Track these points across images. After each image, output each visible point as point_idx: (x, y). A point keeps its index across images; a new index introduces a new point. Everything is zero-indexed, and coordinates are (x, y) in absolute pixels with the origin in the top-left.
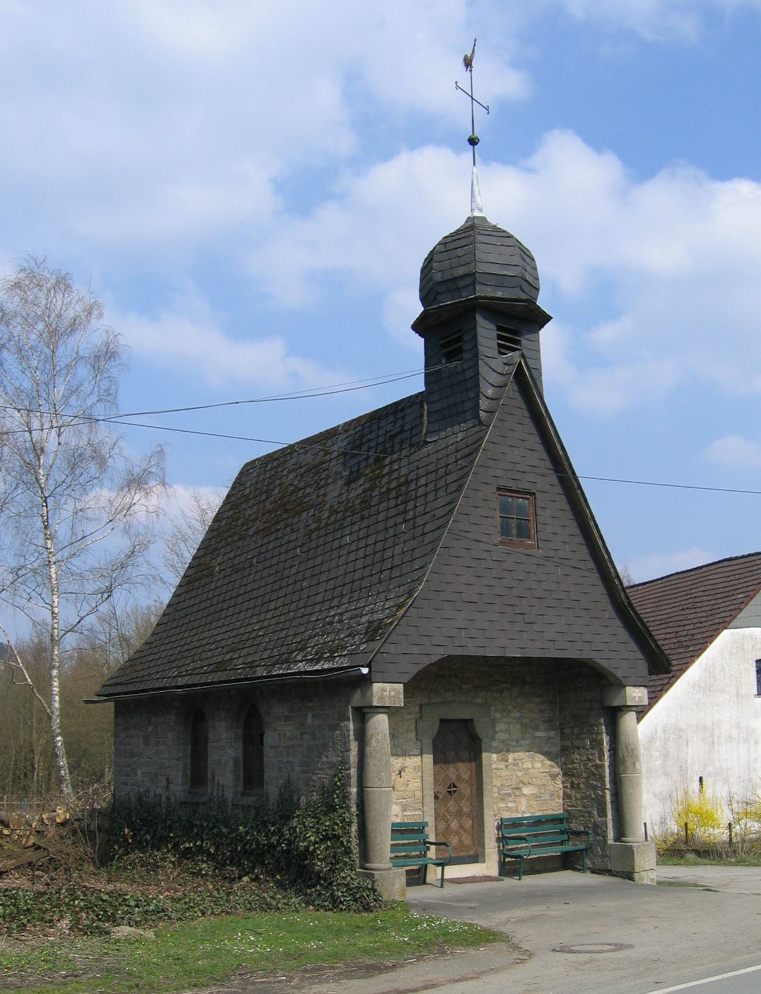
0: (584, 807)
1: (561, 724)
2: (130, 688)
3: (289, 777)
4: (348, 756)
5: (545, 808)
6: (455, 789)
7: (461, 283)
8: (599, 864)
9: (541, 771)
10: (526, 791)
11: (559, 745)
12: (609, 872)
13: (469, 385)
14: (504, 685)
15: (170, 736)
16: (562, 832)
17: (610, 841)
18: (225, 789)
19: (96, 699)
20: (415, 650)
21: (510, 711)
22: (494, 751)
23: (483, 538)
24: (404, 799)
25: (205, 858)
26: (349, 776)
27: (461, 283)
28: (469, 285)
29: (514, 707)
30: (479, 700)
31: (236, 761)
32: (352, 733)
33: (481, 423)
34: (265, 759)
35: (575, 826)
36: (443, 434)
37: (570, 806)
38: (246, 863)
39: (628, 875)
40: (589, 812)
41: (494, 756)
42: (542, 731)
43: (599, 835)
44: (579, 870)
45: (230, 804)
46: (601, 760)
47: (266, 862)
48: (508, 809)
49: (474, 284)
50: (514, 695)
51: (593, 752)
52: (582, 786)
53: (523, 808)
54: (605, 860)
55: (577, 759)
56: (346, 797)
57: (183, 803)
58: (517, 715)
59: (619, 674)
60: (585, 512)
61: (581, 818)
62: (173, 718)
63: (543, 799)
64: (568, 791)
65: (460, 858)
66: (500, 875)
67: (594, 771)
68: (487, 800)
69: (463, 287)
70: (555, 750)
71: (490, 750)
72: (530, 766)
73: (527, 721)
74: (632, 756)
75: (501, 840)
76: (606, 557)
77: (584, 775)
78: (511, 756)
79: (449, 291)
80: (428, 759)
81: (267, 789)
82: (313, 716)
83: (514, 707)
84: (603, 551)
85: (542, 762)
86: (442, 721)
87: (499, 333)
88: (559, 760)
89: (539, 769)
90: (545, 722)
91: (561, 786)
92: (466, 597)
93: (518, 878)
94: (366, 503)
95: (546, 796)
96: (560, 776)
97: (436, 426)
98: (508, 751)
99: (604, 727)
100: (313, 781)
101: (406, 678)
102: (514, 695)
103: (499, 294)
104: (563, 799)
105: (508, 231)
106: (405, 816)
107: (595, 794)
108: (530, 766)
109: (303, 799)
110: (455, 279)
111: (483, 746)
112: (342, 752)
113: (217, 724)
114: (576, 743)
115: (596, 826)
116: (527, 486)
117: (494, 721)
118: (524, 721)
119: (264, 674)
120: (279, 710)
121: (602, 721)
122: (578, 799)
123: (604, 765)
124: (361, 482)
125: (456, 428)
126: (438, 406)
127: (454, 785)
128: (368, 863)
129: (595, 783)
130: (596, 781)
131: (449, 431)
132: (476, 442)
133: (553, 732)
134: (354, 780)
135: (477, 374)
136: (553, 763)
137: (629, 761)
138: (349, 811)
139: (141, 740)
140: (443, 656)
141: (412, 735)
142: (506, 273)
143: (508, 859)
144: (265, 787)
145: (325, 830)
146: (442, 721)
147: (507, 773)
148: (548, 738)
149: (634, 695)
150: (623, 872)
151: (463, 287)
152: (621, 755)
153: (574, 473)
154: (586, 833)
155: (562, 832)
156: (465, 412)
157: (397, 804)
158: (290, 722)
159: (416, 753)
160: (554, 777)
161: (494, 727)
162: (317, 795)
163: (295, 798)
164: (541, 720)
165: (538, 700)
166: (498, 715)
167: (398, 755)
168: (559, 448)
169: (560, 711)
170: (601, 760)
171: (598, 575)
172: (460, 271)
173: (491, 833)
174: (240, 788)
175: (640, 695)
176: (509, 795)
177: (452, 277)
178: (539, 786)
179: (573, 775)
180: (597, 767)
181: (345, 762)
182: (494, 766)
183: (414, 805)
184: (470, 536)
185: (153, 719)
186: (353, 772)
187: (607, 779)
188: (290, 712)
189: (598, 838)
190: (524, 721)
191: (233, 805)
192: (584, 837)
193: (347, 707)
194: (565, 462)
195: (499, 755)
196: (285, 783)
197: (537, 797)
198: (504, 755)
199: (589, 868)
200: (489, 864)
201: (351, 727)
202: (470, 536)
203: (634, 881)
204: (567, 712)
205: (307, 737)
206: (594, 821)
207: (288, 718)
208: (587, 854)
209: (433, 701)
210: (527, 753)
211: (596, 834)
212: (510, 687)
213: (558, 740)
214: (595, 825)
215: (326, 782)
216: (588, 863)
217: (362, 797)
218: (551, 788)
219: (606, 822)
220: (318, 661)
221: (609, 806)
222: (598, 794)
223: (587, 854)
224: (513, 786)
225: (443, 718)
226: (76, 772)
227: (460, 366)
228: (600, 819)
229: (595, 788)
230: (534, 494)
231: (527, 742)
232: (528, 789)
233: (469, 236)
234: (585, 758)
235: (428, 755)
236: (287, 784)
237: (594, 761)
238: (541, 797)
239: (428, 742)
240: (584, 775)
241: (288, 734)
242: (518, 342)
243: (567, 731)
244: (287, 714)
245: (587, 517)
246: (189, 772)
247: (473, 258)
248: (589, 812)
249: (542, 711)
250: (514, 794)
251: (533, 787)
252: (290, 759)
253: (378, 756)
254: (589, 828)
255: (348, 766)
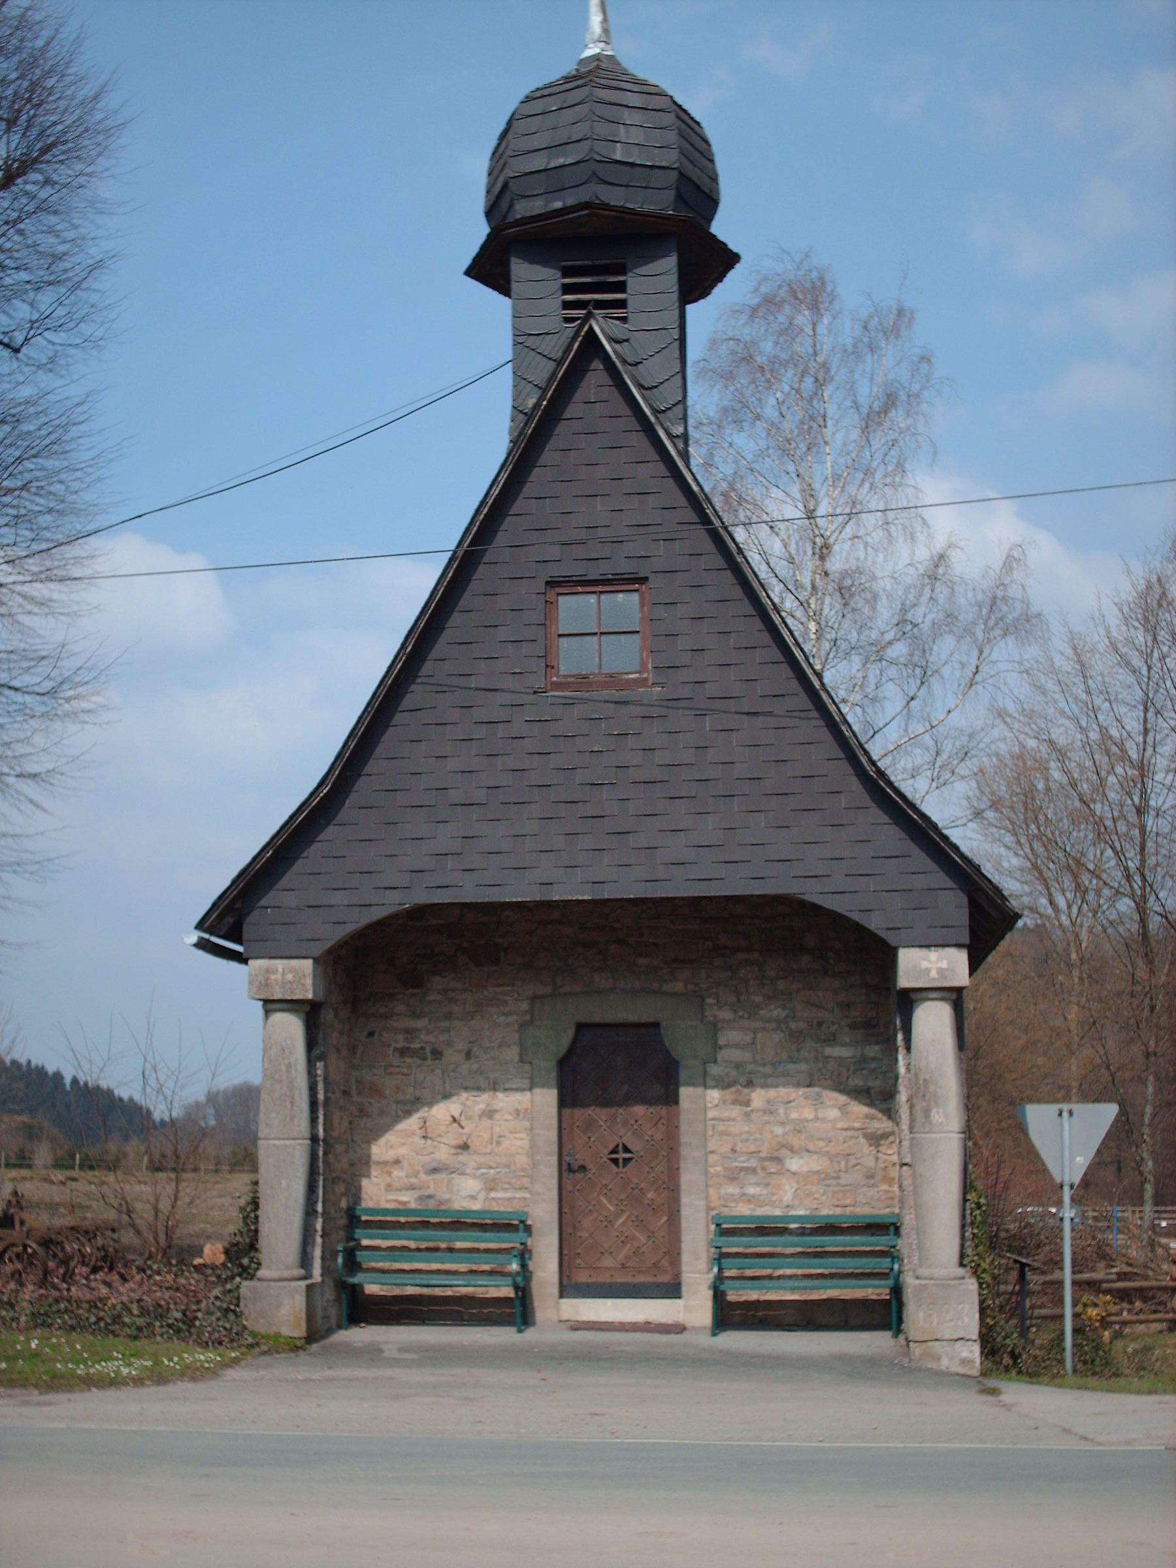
5: (848, 1202)
6: (627, 1155)
9: (839, 1125)
14: (741, 956)
20: (338, 898)
21: (758, 1006)
22: (713, 1083)
23: (508, 683)
24: (491, 1168)
29: (770, 998)
30: (678, 987)
41: (714, 1095)
42: (844, 1045)
48: (750, 1199)
53: (788, 1198)
58: (777, 1012)
63: (842, 1182)
65: (634, 1286)
71: (704, 1081)
73: (802, 1025)
74: (924, 1096)
78: (759, 1097)
80: (547, 1098)
85: (842, 1108)
86: (581, 1027)
87: (567, 280)
89: (834, 1121)
90: (853, 1026)
92: (455, 796)
98: (750, 1084)
101: (319, 949)
102: (772, 974)
106: (494, 1199)
108: (811, 1116)
111: (683, 1076)
116: (626, 567)
117: (715, 1028)
118: (793, 1025)
127: (613, 1152)
133: (877, 1048)
136: (873, 1111)
140: (401, 908)
141: (513, 1053)
142: (561, 161)
146: (581, 1027)
147: (746, 1128)
149: (925, 964)
157: (475, 1177)
159: (524, 1086)
164: (843, 1023)
165: (837, 984)
166: (725, 1014)
167: (478, 1089)
175: (944, 965)
176: (753, 1170)
178: (831, 1157)
182: (710, 1114)
183: (514, 1181)
184: (473, 682)
190: (793, 1025)
195: (727, 1091)
197: (822, 1177)
198: (739, 1092)
200: (692, 1303)
202: (473, 682)
209: (562, 990)
210: (801, 1091)
212: (761, 960)
218: (869, 1162)
224: (762, 1155)
225: (583, 1020)
226: (775, 1198)
231: (803, 1067)
232: (801, 1161)
235: (545, 1091)
238: (838, 1178)
239: (547, 1065)
242: (621, 287)
249: (846, 1006)
250: (764, 1169)
251: (815, 1157)
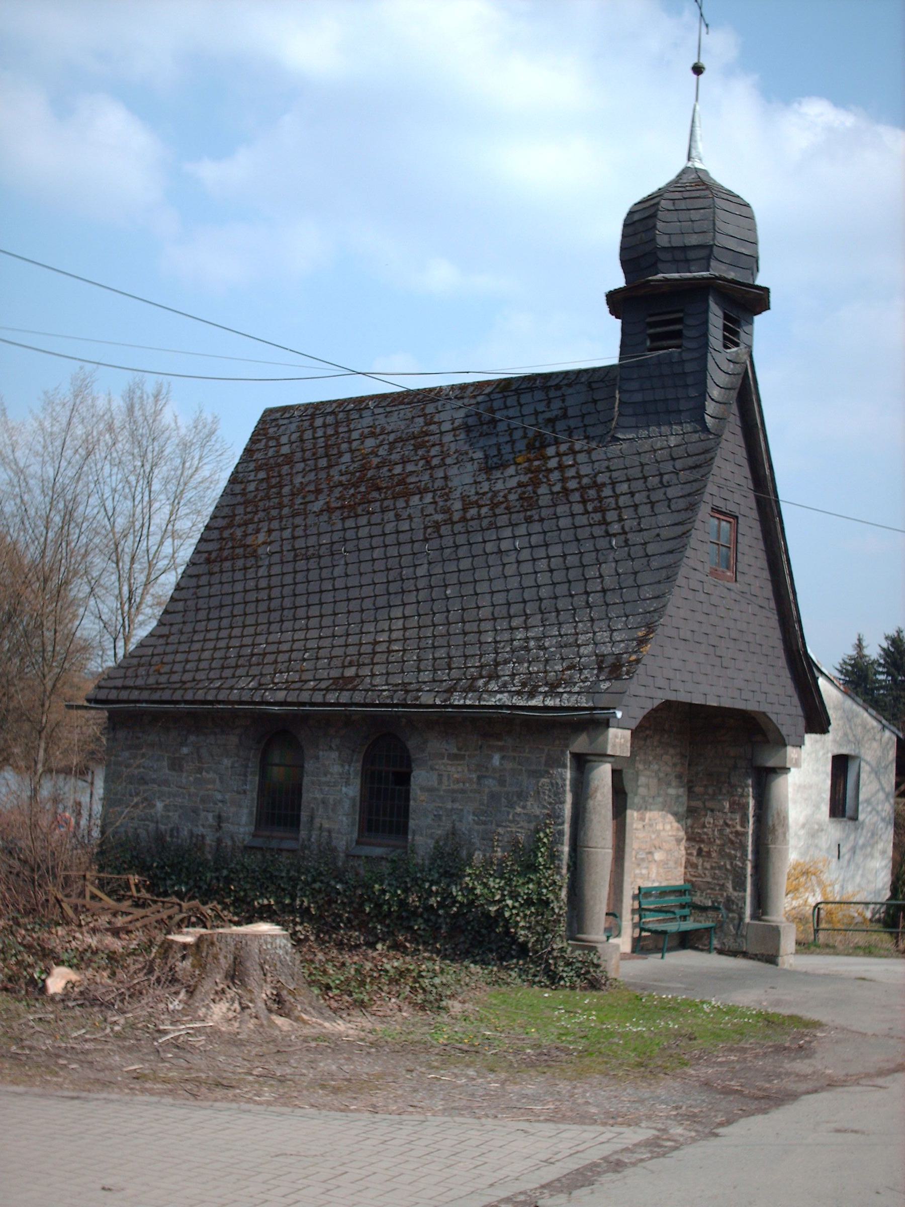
0: (713, 878)
1: (690, 781)
2: (156, 696)
3: (453, 827)
4: (562, 810)
7: (691, 255)
8: (730, 943)
10: (658, 856)
11: (686, 805)
12: (745, 955)
13: (690, 380)
14: (648, 732)
15: (227, 762)
16: (683, 906)
17: (747, 919)
18: (334, 835)
19: (86, 704)
25: (298, 920)
26: (561, 833)
27: (691, 255)
28: (702, 258)
31: (353, 799)
32: (568, 782)
33: (706, 429)
34: (412, 803)
35: (698, 899)
36: (643, 433)
37: (695, 876)
38: (379, 927)
39: (771, 959)
40: (723, 885)
43: (732, 911)
44: (702, 950)
45: (342, 855)
46: (743, 826)
47: (416, 927)
48: (642, 876)
49: (708, 258)
50: (655, 744)
51: (733, 817)
52: (714, 855)
54: (739, 940)
55: (709, 823)
56: (554, 856)
57: (248, 849)
58: (656, 767)
59: (784, 731)
60: (779, 543)
61: (709, 891)
62: (234, 740)
64: (694, 859)
66: (633, 951)
67: (733, 838)
68: (627, 864)
69: (694, 260)
70: (682, 809)
71: (631, 808)
72: (661, 828)
75: (640, 911)
76: (791, 597)
77: (718, 842)
78: (648, 815)
79: (675, 261)
81: (413, 839)
82: (503, 758)
83: (654, 758)
84: (790, 590)
88: (684, 823)
91: (684, 852)
93: (660, 955)
94: (529, 502)
95: (671, 864)
96: (684, 841)
97: (632, 421)
98: (646, 809)
99: (751, 790)
100: (499, 834)
102: (655, 744)
103: (731, 275)
104: (686, 868)
105: (742, 196)
107: (731, 864)
108: (661, 828)
109: (478, 856)
110: (685, 248)
112: (550, 803)
113: (321, 753)
114: (709, 804)
115: (729, 900)
119: (438, 702)
120: (436, 745)
121: (750, 782)
122: (706, 869)
123: (747, 833)
124: (511, 470)
125: (665, 429)
126: (638, 397)
128: (583, 933)
129: (733, 852)
130: (734, 849)
131: (654, 431)
132: (703, 453)
134: (566, 838)
135: (704, 370)
137: (780, 831)
138: (559, 873)
139: (165, 763)
143: (644, 934)
144: (410, 837)
145: (527, 894)
148: (678, 796)
150: (763, 955)
151: (694, 260)
152: (770, 823)
153: (777, 496)
154: (715, 909)
155: (683, 906)
156: (680, 412)
158: (462, 762)
160: (679, 841)
161: (637, 780)
162: (503, 851)
163: (464, 853)
168: (767, 466)
169: (689, 765)
170: (743, 826)
171: (777, 617)
172: (693, 240)
173: (628, 904)
174: (355, 835)
176: (643, 859)
177: (682, 245)
179: (702, 841)
180: (737, 833)
181: (556, 816)
185: (192, 738)
186: (567, 828)
187: (750, 849)
188: (459, 749)
189: (730, 915)
191: (347, 856)
192: (711, 914)
193: (563, 753)
194: (770, 485)
196: (447, 835)
197: (665, 863)
199: (715, 949)
201: (568, 774)
203: (777, 965)
204: (700, 769)
205: (490, 782)
206: (727, 896)
207: (454, 757)
208: (715, 933)
211: (729, 910)
213: (685, 799)
214: (729, 900)
215: (521, 837)
216: (715, 943)
217: (576, 857)
218: (676, 854)
219: (744, 898)
220: (532, 695)
221: (749, 881)
222: (736, 865)
223: (715, 933)
227: (676, 354)
228: (736, 894)
229: (732, 858)
230: (737, 517)
233: (705, 197)
234: (721, 822)
236: (450, 836)
237: (734, 827)
240: (718, 842)
241: (455, 776)
243: (698, 789)
244: (455, 751)
245: (780, 548)
246: (255, 809)
247: (711, 227)
248: (723, 885)
252: (457, 805)
253: (603, 812)
254: (719, 903)
255: (560, 820)
